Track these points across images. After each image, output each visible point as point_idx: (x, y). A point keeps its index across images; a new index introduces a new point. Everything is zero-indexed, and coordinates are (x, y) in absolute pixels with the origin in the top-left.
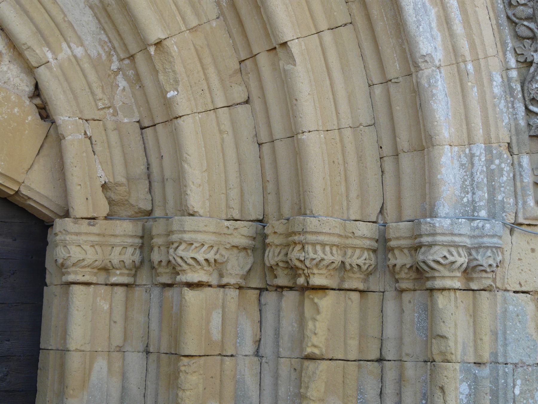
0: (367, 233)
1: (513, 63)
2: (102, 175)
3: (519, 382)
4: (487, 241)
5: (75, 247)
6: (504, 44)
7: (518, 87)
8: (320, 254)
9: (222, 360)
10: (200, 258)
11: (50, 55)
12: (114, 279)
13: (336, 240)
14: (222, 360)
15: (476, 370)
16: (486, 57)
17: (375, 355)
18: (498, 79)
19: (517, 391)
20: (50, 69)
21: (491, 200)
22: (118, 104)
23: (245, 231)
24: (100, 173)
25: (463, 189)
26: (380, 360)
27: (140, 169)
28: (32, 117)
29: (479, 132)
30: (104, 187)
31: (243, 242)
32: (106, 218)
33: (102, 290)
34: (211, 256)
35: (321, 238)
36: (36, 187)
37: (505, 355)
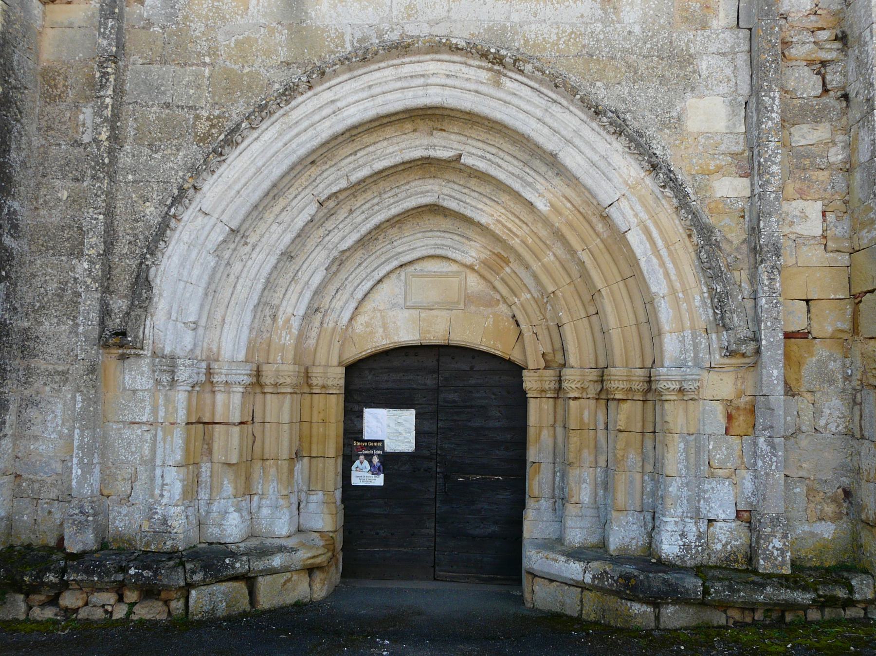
0: (642, 374)
1: (705, 290)
2: (542, 350)
3: (712, 443)
4: (688, 377)
5: (530, 382)
6: (700, 281)
7: (709, 301)
8: (617, 385)
9: (227, 432)
10: (573, 387)
11: (516, 300)
12: (548, 396)
13: (625, 378)
14: (227, 432)
15: (688, 437)
16: (163, 465)
17: (652, 430)
18: (698, 298)
19: (711, 447)
20: (516, 306)
21: (696, 356)
22: (548, 317)
23: (595, 374)
24: (541, 348)
25: (681, 351)
26: (654, 432)
27: (558, 345)
28: (513, 326)
29: (688, 324)
30: (543, 355)
31: (595, 378)
32: (544, 368)
33: (544, 400)
34: (578, 385)
35: (617, 378)
36: (516, 356)
37: (704, 430)
